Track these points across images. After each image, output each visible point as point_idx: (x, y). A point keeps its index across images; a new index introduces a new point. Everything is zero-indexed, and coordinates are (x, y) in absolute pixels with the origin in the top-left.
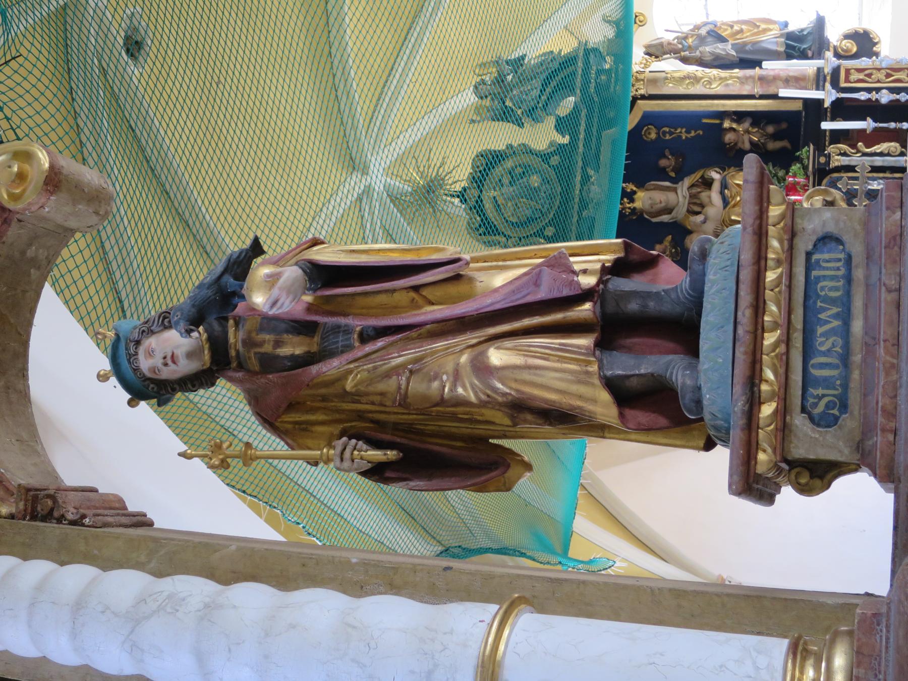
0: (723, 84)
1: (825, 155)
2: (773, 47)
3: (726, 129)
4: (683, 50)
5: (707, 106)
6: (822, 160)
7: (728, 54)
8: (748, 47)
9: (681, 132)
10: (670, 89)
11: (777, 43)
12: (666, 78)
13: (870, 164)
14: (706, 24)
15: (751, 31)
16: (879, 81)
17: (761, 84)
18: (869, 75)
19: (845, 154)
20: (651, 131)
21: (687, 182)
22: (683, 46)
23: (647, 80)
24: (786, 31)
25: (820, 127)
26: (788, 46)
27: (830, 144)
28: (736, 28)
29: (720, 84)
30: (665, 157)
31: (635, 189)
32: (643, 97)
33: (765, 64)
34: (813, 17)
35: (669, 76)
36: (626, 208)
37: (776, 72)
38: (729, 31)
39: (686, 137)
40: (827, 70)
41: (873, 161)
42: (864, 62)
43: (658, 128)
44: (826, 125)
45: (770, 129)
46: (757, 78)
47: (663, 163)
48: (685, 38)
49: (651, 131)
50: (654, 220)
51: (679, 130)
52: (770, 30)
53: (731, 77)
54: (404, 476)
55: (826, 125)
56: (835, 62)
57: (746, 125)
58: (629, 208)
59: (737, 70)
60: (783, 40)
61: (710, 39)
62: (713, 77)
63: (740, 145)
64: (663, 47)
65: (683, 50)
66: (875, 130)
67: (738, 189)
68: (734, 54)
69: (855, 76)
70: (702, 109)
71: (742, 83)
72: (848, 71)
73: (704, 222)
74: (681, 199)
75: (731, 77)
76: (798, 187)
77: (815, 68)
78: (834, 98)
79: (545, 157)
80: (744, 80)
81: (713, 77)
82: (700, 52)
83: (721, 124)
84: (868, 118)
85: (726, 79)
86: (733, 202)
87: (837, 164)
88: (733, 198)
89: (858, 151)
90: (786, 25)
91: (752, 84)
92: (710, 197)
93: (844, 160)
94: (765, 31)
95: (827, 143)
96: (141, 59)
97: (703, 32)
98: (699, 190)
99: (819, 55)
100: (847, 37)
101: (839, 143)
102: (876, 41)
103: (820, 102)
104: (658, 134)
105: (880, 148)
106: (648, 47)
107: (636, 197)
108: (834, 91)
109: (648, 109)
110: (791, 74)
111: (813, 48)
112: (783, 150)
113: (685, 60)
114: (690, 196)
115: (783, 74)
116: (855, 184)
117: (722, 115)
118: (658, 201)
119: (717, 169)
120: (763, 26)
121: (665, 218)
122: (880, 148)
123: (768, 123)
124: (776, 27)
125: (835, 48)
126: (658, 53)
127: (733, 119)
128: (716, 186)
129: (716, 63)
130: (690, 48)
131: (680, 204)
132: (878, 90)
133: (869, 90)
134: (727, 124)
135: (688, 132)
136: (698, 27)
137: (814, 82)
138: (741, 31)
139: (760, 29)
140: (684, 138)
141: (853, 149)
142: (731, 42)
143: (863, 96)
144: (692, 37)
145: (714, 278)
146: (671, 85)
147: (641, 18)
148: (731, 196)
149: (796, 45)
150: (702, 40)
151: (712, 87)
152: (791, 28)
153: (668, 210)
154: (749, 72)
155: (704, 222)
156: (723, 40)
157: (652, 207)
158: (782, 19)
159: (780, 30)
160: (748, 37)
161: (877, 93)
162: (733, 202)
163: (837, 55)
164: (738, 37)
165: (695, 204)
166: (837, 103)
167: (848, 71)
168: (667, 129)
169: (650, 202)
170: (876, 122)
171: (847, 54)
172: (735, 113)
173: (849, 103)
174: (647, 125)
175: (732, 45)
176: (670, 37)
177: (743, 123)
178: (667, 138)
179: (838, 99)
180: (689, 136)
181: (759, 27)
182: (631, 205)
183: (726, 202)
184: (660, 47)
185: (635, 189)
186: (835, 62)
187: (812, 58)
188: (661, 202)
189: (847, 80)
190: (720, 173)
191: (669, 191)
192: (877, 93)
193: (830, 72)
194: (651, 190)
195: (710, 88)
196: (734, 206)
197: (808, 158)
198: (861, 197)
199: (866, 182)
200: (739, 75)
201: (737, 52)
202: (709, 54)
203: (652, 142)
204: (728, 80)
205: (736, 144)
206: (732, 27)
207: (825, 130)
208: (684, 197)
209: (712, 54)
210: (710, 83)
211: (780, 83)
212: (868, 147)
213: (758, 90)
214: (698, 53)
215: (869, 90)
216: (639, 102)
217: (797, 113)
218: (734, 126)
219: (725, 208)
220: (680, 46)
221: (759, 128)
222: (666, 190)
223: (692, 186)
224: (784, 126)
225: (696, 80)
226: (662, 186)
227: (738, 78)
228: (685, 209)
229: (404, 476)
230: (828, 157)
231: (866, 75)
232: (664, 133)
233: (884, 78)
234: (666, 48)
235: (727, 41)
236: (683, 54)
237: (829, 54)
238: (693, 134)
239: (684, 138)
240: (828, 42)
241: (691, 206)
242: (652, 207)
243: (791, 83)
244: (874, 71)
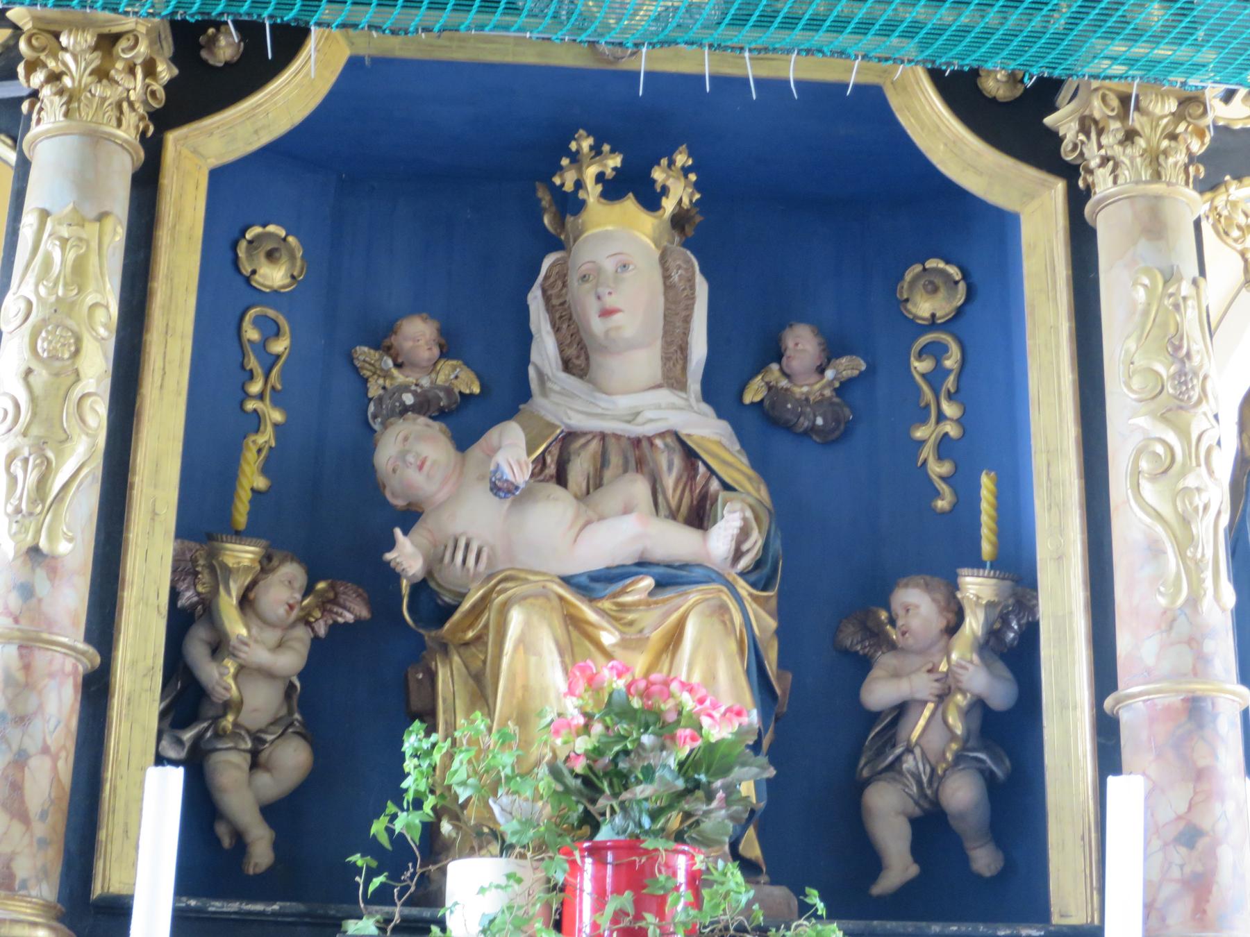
0: (1159, 529)
3: (953, 586)
9: (941, 417)
20: (942, 293)
23: (1158, 198)
29: (1159, 517)
30: (833, 350)
32: (1077, 199)
35: (1186, 288)
36: (580, 171)
39: (921, 443)
46: (1198, 687)
49: (942, 293)
50: (535, 299)
51: (949, 409)
53: (1192, 568)
58: (579, 184)
59: (1229, 596)
62: (1190, 481)
63: (885, 661)
67: (656, 636)
71: (1169, 620)
73: (501, 489)
74: (624, 403)
75: (1192, 568)
76: (451, 751)
80: (1182, 626)
85: (1185, 543)
88: (616, 618)
98: (669, 481)
104: (932, 324)
107: (629, 204)
112: (873, 862)
114: (637, 442)
119: (755, 541)
127: (1004, 620)
131: (603, 402)
135: (944, 447)
140: (919, 434)
145: (633, 858)
146: (1141, 294)
148: (623, 607)
151: (1147, 488)
155: (501, 489)
157: (584, 278)
165: (603, 461)
168: (951, 362)
169: (609, 265)
172: (1031, 634)
174: (966, 276)
180: (927, 452)
182: (592, 191)
185: (669, 205)
188: (606, 313)
190: (738, 555)
191: (666, 359)
194: (666, 277)
195: (1136, 473)
196: (574, 621)
200: (1207, 603)
203: (897, 305)
204: (1181, 554)
205: (893, 646)
208: (633, 416)
210: (1166, 469)
211: (1176, 802)
216: (1060, 186)
218: (974, 624)
219: (567, 581)
222: (667, 343)
224: (984, 860)
226: (687, 320)
227: (1194, 601)
228: (578, 421)
232: (936, 351)
238: (938, 469)
239: (919, 434)
241: (595, 445)
242: (584, 278)
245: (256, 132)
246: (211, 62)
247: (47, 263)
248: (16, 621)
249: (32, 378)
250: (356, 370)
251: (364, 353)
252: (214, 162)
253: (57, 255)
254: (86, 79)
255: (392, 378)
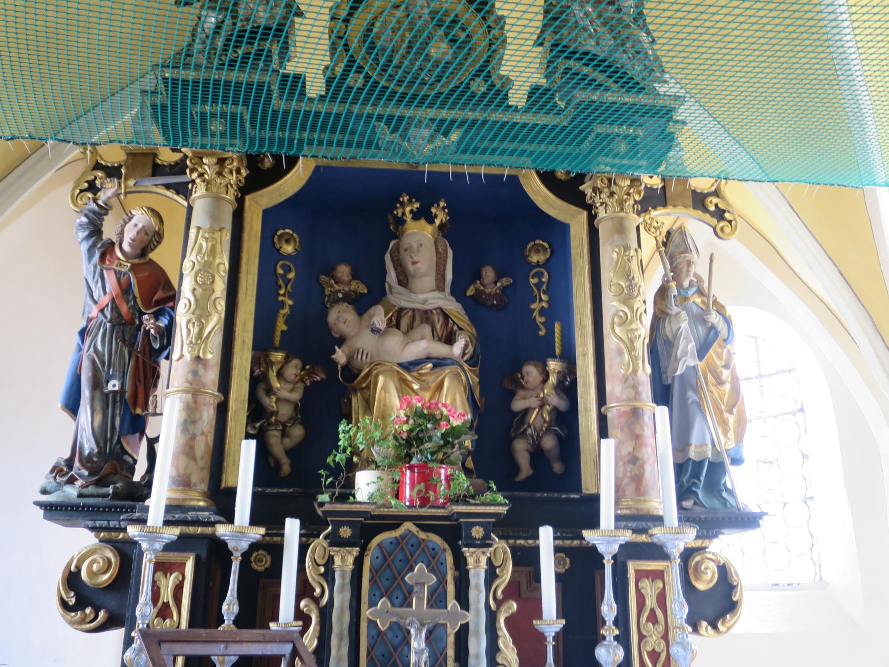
0: (622, 344)
1: (487, 536)
2: (695, 438)
4: (679, 286)
5: (582, 327)
6: (477, 532)
7: (677, 361)
8: (692, 396)
9: (541, 300)
10: (608, 255)
11: (704, 444)
12: (627, 248)
13: (472, 627)
14: (727, 321)
15: (722, 400)
16: (641, 637)
17: (625, 412)
18: (653, 618)
19: (491, 575)
21: (453, 306)
22: (687, 289)
23: (622, 218)
24: (728, 461)
25: (543, 524)
26: (699, 465)
27: (513, 549)
28: (725, 374)
30: (499, 276)
31: (437, 222)
32: (592, 218)
33: (662, 412)
34: (754, 509)
35: (632, 253)
36: (404, 209)
37: (651, 441)
38: (719, 363)
39: (534, 310)
40: (658, 534)
41: (477, 633)
42: (679, 608)
43: (546, 264)
44: (546, 535)
45: (549, 443)
46: (637, 404)
47: (489, 273)
48: (700, 292)
50: (388, 258)
51: (544, 297)
52: (725, 433)
53: (635, 360)
54: (601, 619)
55: (546, 535)
56: (676, 548)
57: (556, 400)
58: (404, 214)
59: (649, 369)
60: (709, 455)
61: (702, 330)
62: (634, 326)
63: (521, 393)
64: (683, 253)
65: (679, 286)
66: (542, 637)
67: (433, 385)
68: (679, 372)
69: (650, 589)
70: (577, 318)
71: (625, 379)
72: (659, 575)
73: (375, 331)
74: (421, 297)
77: (661, 513)
78: (601, 549)
79: (485, 70)
81: (634, 326)
82: (678, 313)
83: (553, 356)
84: (564, 622)
85: (631, 349)
86: (409, 378)
87: (471, 561)
88: (418, 379)
89: (499, 603)
90: (737, 461)
91: (624, 396)
92: (422, 338)
93: (477, 575)
94: (724, 423)
95: (511, 541)
96: (687, 175)
97: (714, 318)
99: (686, 517)
100: (723, 570)
101: (514, 565)
102: (719, 625)
103: (594, 523)
104: (538, 265)
105: (506, 646)
106: (682, 232)
107: (423, 222)
108: (615, 548)
109: (573, 231)
110: (648, 468)
111: (698, 509)
113: (662, 293)
114: (426, 312)
115: (647, 452)
116: (420, 599)
117: (569, 359)
118: (416, 259)
119: (470, 349)
120: (731, 420)
121: (392, 276)
122: (506, 646)
123: (560, 440)
124: (731, 445)
125: (702, 549)
126: (671, 246)
127: (565, 377)
128: (440, 349)
129: (660, 345)
130: (684, 299)
131: (414, 296)
132: (624, 640)
133: (622, 621)
134: (554, 365)
135: (542, 312)
136: (721, 310)
137: (633, 512)
138: (720, 382)
139: (726, 415)
140: (533, 307)
141: (503, 592)
142: (701, 365)
143: (608, 609)
144: (703, 302)
146: (615, 255)
147: (728, 230)
148: (421, 375)
149: (702, 479)
150: (700, 318)
151: (617, 329)
152: (732, 469)
153: (404, 280)
154: (646, 391)
156: (702, 351)
157: (406, 250)
158: (747, 452)
159: (727, 451)
160: (710, 393)
161: (616, 638)
162: (409, 378)
163: (688, 554)
164: (709, 376)
165: (413, 319)
166: (593, 556)
167: (659, 575)
168: (545, 279)
169: (415, 245)
170: (555, 639)
171: (691, 572)
173: (598, 578)
174: (550, 247)
175: (694, 368)
176: (700, 267)
177: (558, 394)
178: (531, 280)
179: (602, 557)
180: (536, 314)
181: (730, 412)
183: (411, 366)
184: (682, 249)
185: (437, 222)
186: (676, 548)
187: (680, 508)
188: (414, 263)
189: (641, 575)
190: (464, 354)
191: (437, 280)
192: (616, 638)
193: (655, 540)
194: (437, 249)
195: (613, 323)
196: (403, 380)
197: (483, 504)
198: (393, 614)
199: (423, 625)
201: (682, 376)
202: (674, 329)
204: (630, 354)
205: (523, 387)
206: (726, 366)
207: (536, 537)
208: (425, 302)
209: (677, 335)
211: (628, 448)
212: (507, 620)
213: (613, 409)
214: (675, 309)
215: (622, 621)
216: (585, 213)
217: (577, 485)
218: (553, 379)
219: (400, 365)
220: (686, 284)
221: (550, 423)
222: (437, 270)
223: (446, 316)
224: (558, 467)
225: (628, 296)
226: (445, 265)
227: (635, 371)
228: (404, 304)
229: (601, 619)
230: (484, 543)
231: (652, 611)
232: (539, 275)
233: (649, 649)
234: (680, 259)
235: (701, 359)
236: (673, 284)
237: (689, 537)
238: (540, 320)
239: (533, 307)
240: (711, 537)
241: (410, 313)
242: (406, 250)
243: (629, 468)
244: (661, 628)
245: (280, 195)
246: (262, 168)
247: (201, 247)
248: (191, 384)
249: (195, 292)
250: (320, 284)
251: (323, 278)
252: (265, 207)
253: (204, 244)
254: (214, 176)
255: (334, 287)
